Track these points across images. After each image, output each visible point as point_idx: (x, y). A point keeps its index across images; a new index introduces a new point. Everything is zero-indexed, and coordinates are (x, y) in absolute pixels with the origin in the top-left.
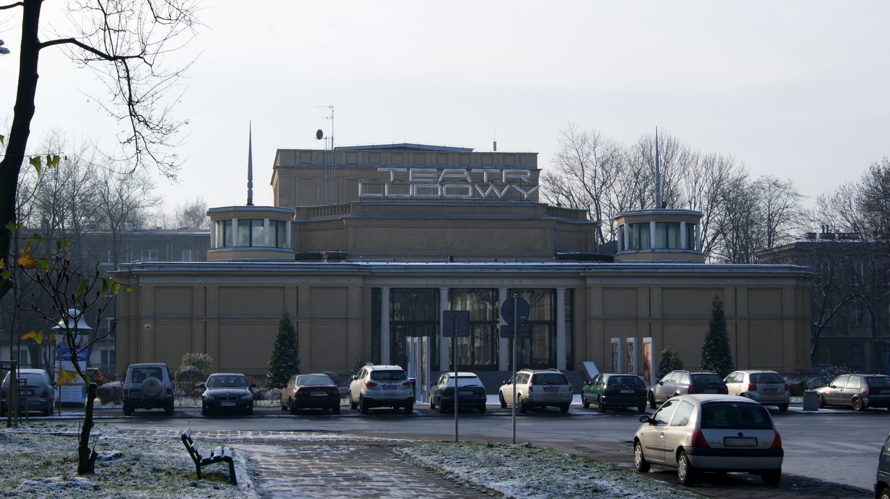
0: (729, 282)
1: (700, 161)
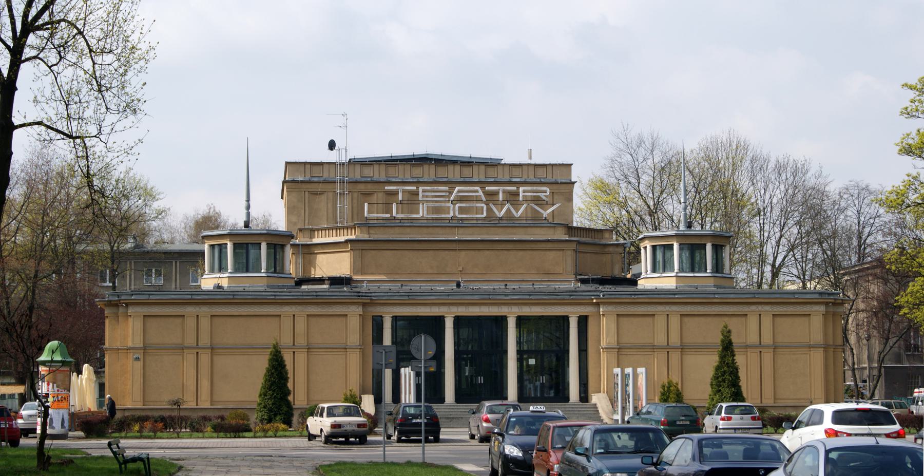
0: (753, 308)
1: (772, 165)
